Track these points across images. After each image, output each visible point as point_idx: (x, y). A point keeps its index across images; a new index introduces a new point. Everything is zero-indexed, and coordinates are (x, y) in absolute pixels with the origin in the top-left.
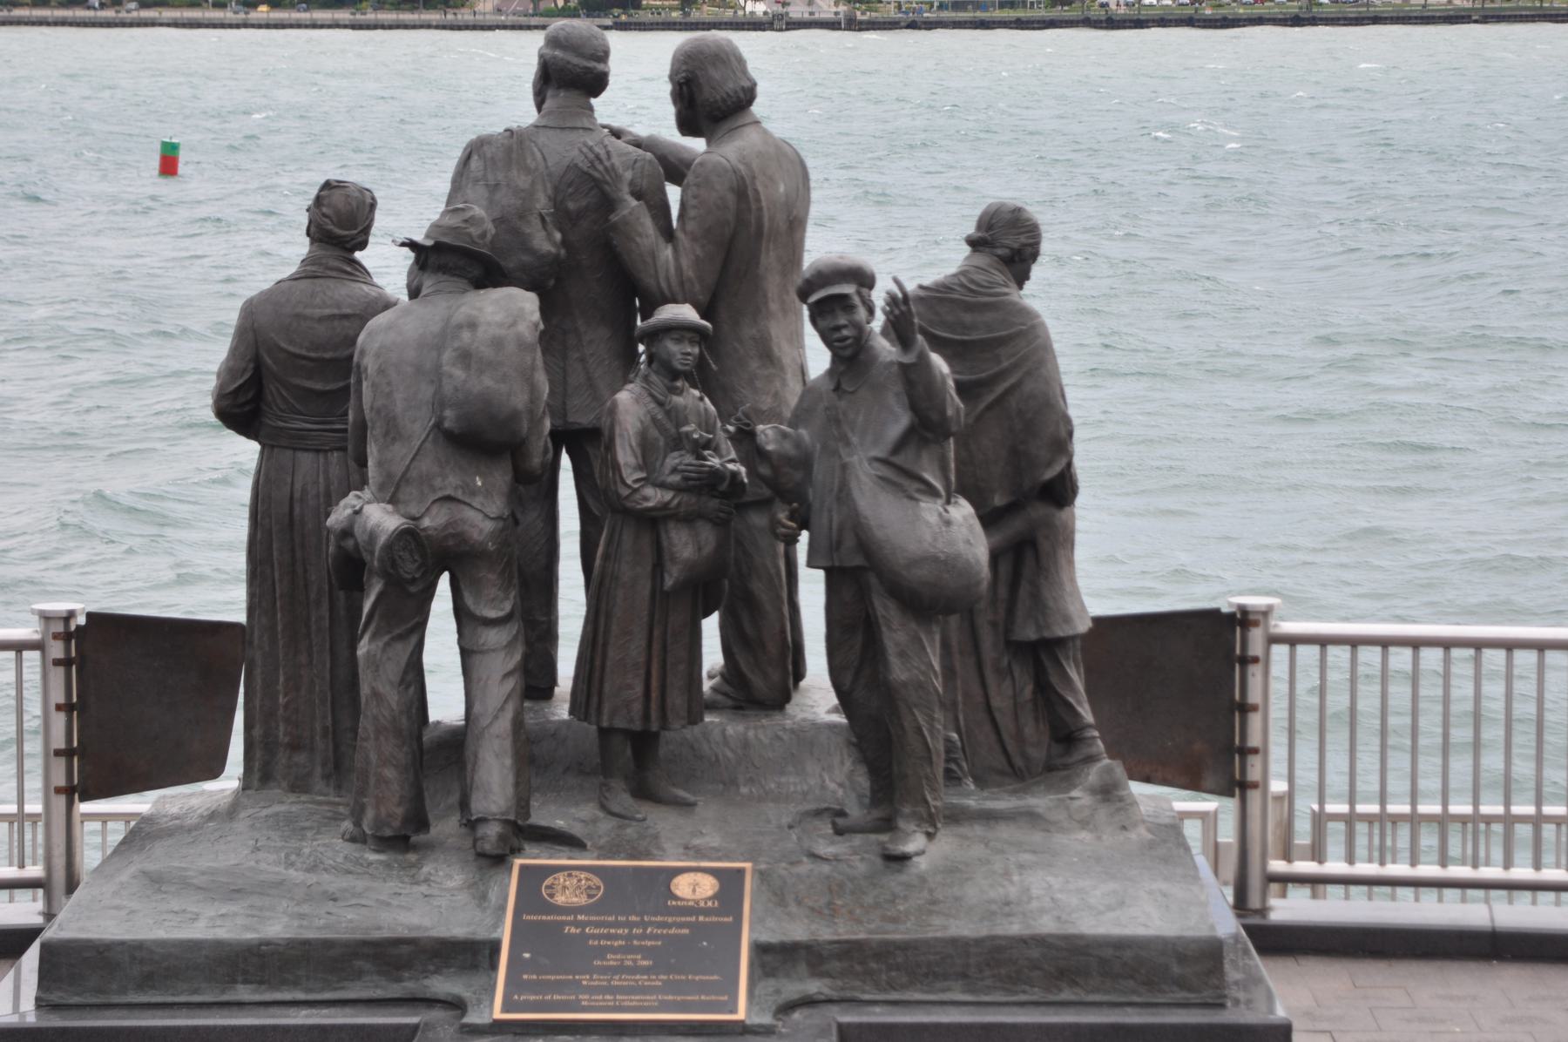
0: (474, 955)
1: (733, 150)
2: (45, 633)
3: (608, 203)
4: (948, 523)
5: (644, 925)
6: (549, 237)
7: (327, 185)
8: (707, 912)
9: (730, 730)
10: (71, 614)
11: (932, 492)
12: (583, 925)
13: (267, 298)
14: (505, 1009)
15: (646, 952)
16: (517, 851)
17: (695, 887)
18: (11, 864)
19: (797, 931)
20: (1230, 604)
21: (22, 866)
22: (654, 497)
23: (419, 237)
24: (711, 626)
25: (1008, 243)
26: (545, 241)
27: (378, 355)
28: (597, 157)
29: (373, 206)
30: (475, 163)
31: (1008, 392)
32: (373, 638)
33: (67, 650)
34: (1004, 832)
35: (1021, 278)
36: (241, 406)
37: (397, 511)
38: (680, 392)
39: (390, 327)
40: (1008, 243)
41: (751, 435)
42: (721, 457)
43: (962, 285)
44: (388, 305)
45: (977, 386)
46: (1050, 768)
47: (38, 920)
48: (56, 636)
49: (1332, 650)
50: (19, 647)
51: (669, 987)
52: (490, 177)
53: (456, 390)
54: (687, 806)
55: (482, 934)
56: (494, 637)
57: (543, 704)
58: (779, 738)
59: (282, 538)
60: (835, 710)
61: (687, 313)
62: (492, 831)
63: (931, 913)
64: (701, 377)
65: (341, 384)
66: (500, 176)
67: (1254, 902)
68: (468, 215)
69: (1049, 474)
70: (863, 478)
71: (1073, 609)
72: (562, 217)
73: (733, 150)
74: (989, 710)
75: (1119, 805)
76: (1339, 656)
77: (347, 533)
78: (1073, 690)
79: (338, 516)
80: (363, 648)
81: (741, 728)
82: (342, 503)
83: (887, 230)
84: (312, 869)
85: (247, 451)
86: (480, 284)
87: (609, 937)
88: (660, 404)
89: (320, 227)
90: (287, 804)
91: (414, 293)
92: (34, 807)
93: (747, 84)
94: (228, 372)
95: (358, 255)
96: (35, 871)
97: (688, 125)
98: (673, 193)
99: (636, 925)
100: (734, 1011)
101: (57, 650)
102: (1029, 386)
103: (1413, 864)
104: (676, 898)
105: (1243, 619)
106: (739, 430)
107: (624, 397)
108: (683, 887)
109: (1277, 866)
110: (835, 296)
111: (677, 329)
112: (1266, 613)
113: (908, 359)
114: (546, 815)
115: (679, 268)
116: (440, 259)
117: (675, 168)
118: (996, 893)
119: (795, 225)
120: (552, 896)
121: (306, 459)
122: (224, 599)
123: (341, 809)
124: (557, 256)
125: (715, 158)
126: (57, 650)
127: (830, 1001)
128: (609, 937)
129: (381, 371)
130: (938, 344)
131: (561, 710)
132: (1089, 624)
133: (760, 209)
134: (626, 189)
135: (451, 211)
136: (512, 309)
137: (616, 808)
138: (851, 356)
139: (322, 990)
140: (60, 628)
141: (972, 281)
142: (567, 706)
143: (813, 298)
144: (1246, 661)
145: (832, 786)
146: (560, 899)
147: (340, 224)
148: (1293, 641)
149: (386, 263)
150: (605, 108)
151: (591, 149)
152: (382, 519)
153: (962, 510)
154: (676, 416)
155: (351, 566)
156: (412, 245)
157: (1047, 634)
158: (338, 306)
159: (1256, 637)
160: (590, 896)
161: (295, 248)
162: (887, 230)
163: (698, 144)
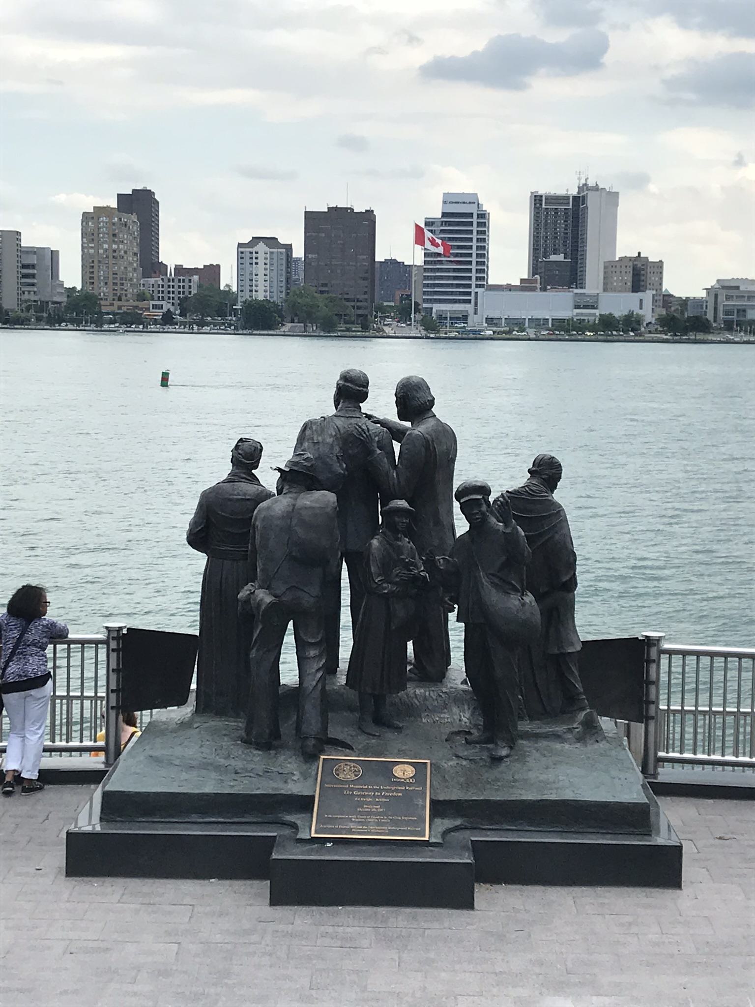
0: (304, 804)
1: (423, 428)
2: (108, 637)
3: (371, 452)
4: (523, 605)
5: (379, 790)
6: (341, 465)
7: (241, 440)
8: (410, 784)
9: (418, 692)
10: (121, 628)
11: (517, 590)
12: (352, 790)
13: (212, 489)
14: (316, 832)
15: (383, 804)
16: (322, 751)
17: (404, 771)
18: (91, 740)
19: (455, 795)
20: (643, 636)
21: (95, 741)
22: (387, 588)
23: (282, 467)
24: (410, 645)
25: (547, 472)
26: (340, 468)
27: (263, 520)
28: (363, 430)
29: (261, 450)
30: (308, 432)
31: (547, 541)
32: (257, 650)
33: (118, 644)
34: (543, 743)
35: (553, 487)
36: (198, 538)
37: (271, 594)
38: (399, 539)
39: (269, 508)
40: (547, 472)
41: (434, 561)
42: (418, 569)
43: (527, 492)
44: (269, 495)
45: (530, 534)
46: (563, 712)
47: (102, 767)
48: (113, 638)
49: (688, 658)
50: (97, 642)
51: (394, 822)
52: (315, 438)
53: (534, 896)
54: (399, 729)
55: (306, 793)
56: (312, 653)
57: (332, 676)
58: (440, 696)
59: (215, 595)
60: (464, 682)
61: (403, 503)
62: (311, 742)
63: (513, 787)
64: (409, 533)
65: (245, 530)
66: (320, 438)
67: (651, 771)
68: (305, 457)
69: (565, 579)
70: (485, 583)
71: (575, 639)
72: (345, 456)
73: (423, 428)
74: (536, 685)
75: (594, 731)
76: (691, 660)
77: (247, 601)
78: (575, 678)
79: (243, 594)
80: (253, 654)
81: (422, 691)
82: (246, 588)
83: (490, 463)
84: (227, 757)
85: (200, 560)
86: (310, 489)
87: (364, 796)
88: (391, 545)
89: (237, 459)
90: (215, 723)
91: (280, 492)
92: (102, 693)
93: (430, 398)
94: (194, 524)
95: (253, 471)
96: (101, 743)
97: (401, 416)
98: (397, 446)
99: (378, 797)
100: (424, 836)
101: (113, 645)
102: (557, 537)
103: (723, 755)
104: (396, 777)
105: (649, 642)
106: (427, 559)
107: (375, 542)
108: (398, 771)
109: (661, 754)
110: (474, 497)
111: (399, 511)
112: (659, 640)
113: (508, 531)
114: (334, 732)
115: (399, 482)
116: (293, 477)
117: (397, 434)
118: (543, 777)
119: (450, 460)
120: (338, 775)
121: (227, 563)
122: (185, 621)
123: (240, 725)
124: (344, 475)
125: (416, 432)
126: (113, 645)
127: (466, 828)
128: (364, 796)
129: (264, 527)
130: (520, 520)
131: (342, 680)
132: (578, 647)
133: (436, 455)
134: (375, 445)
135: (296, 455)
136: (324, 499)
137: (367, 731)
138: (477, 524)
139: (232, 817)
140: (115, 635)
141: (531, 490)
142: (344, 677)
143: (462, 501)
144: (649, 661)
145: (464, 719)
146: (341, 776)
147: (246, 457)
148: (671, 653)
149: (267, 476)
150: (366, 407)
151: (360, 427)
152: (264, 597)
153: (529, 598)
154: (399, 550)
155: (249, 614)
156: (279, 470)
157: (563, 651)
158: (245, 494)
159: (654, 652)
160: (356, 776)
161: (225, 469)
162: (490, 463)
163: (408, 424)
